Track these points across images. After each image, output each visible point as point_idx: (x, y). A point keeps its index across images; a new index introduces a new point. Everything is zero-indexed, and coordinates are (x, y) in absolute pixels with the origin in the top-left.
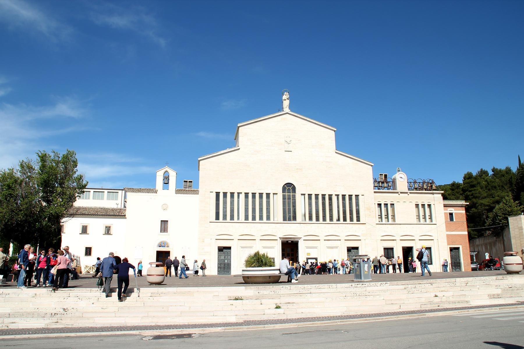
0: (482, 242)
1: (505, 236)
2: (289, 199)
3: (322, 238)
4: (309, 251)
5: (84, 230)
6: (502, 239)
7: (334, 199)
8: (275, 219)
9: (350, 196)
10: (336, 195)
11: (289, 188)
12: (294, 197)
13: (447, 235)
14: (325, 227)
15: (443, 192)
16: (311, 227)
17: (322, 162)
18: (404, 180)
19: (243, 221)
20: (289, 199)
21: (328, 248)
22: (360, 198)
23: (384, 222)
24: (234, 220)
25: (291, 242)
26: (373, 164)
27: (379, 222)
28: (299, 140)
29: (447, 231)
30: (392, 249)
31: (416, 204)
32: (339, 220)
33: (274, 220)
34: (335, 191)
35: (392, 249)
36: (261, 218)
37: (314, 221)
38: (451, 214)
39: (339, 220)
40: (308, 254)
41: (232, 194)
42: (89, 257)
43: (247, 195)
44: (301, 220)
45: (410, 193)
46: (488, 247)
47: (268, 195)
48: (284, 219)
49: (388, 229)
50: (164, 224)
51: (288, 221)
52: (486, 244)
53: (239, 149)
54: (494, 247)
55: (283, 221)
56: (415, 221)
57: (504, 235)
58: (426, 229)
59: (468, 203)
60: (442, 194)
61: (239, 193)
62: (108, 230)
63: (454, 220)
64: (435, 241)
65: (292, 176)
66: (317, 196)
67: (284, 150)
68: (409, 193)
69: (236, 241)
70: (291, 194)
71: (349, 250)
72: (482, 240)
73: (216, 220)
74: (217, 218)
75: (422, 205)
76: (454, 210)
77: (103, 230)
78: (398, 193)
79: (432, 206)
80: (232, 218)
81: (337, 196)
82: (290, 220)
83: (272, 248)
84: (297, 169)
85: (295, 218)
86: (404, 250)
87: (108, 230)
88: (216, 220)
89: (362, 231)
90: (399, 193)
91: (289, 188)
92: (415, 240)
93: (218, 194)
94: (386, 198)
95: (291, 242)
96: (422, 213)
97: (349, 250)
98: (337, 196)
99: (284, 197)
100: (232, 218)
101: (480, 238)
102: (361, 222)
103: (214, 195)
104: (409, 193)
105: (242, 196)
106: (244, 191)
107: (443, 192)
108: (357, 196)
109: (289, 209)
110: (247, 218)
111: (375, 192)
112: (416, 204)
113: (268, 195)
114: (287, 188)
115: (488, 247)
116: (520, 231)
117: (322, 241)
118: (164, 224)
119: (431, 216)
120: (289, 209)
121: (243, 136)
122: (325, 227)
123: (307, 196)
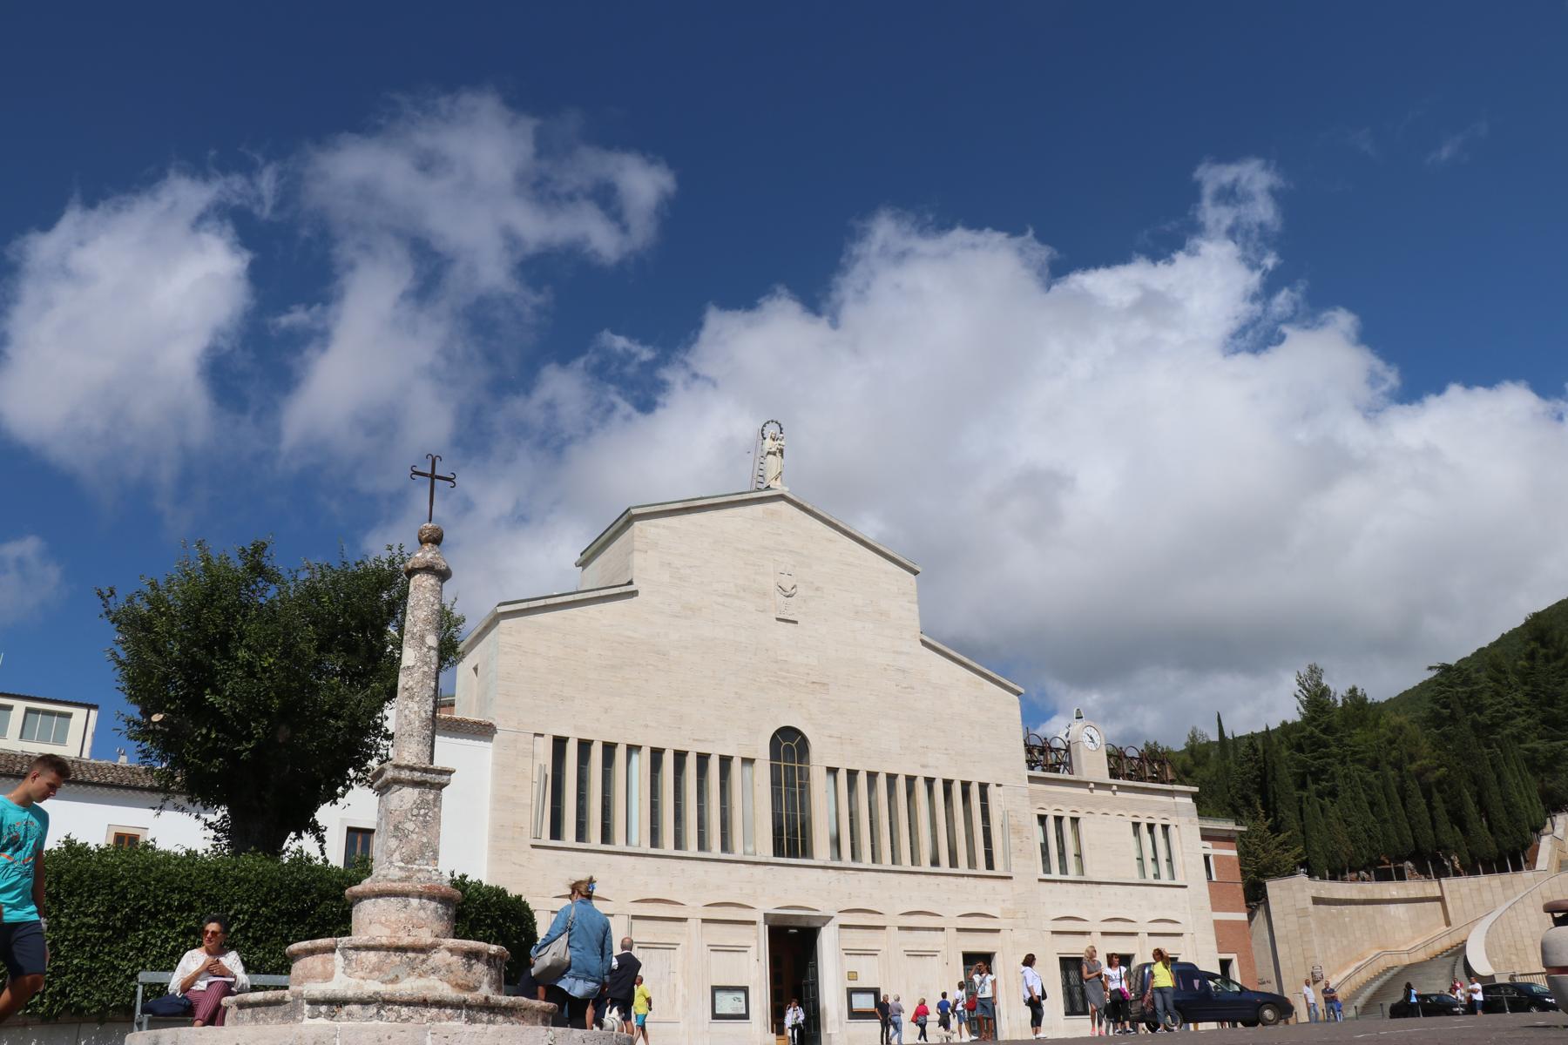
3: (892, 920)
4: (853, 963)
9: (680, 757)
13: (1217, 924)
14: (899, 883)
15: (1196, 789)
16: (859, 881)
18: (1094, 749)
19: (646, 847)
22: (992, 791)
23: (1150, 879)
25: (795, 931)
26: (1022, 690)
29: (1214, 909)
31: (1134, 823)
36: (581, 835)
37: (617, 843)
40: (853, 976)
41: (609, 749)
43: (657, 754)
44: (828, 856)
45: (1122, 788)
47: (725, 761)
48: (778, 851)
49: (1065, 900)
53: (634, 594)
55: (775, 855)
58: (1159, 903)
59: (1244, 829)
60: (1195, 797)
65: (800, 704)
66: (584, 746)
67: (774, 616)
68: (1115, 788)
69: (694, 925)
71: (970, 959)
74: (556, 832)
75: (1072, 818)
79: (1172, 830)
81: (930, 781)
83: (740, 950)
84: (814, 682)
85: (807, 852)
86: (814, 958)
89: (1004, 901)
90: (1092, 785)
92: (1089, 933)
93: (559, 744)
94: (1060, 801)
95: (795, 931)
96: (1148, 855)
97: (970, 959)
98: (930, 781)
99: (775, 770)
100: (606, 836)
102: (999, 869)
103: (545, 750)
104: (1115, 788)
105: (642, 762)
106: (648, 741)
107: (1196, 789)
108: (983, 787)
111: (1032, 779)
112: (1134, 823)
113: (725, 761)
114: (793, 745)
117: (893, 932)
121: (646, 552)
123: (842, 777)
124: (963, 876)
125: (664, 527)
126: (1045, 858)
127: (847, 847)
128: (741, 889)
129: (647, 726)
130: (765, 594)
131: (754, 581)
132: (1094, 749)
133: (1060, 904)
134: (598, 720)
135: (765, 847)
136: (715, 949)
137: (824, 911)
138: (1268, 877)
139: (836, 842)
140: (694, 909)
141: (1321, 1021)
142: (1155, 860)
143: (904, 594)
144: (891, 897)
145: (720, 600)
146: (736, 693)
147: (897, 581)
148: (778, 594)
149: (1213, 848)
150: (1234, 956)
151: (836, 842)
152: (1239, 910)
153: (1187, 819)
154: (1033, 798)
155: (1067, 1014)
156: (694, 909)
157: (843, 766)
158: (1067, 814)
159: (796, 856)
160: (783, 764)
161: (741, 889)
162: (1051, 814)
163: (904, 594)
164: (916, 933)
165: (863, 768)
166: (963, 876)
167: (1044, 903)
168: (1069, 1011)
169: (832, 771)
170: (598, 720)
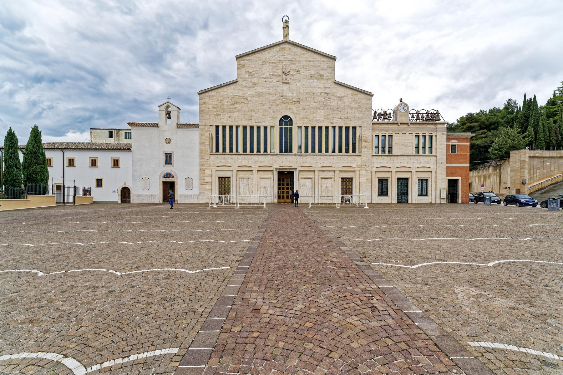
0: (476, 175)
1: (503, 169)
2: (286, 131)
3: (316, 169)
5: (94, 163)
6: (499, 172)
7: (331, 131)
8: (272, 151)
10: (332, 127)
11: (286, 120)
12: (291, 129)
17: (320, 94)
18: (404, 112)
20: (286, 131)
21: (322, 178)
24: (219, 152)
27: (298, 152)
28: (297, 71)
30: (387, 180)
32: (334, 151)
33: (271, 152)
34: (332, 123)
35: (387, 180)
36: (347, 151)
38: (454, 147)
39: (334, 151)
42: (99, 189)
44: (296, 152)
46: (482, 179)
48: (281, 151)
49: (385, 161)
50: (168, 159)
51: (289, 152)
52: (480, 176)
54: (489, 178)
56: (413, 152)
57: (502, 168)
61: (237, 127)
62: (116, 163)
63: (456, 153)
64: (433, 173)
70: (288, 126)
72: (476, 173)
73: (325, 153)
76: (458, 142)
77: (111, 163)
78: (398, 124)
79: (434, 138)
80: (354, 151)
81: (334, 128)
82: (286, 151)
85: (291, 151)
87: (116, 163)
88: (325, 153)
91: (286, 120)
93: (217, 128)
98: (334, 128)
99: (281, 129)
101: (474, 172)
102: (434, 154)
103: (213, 130)
105: (241, 130)
108: (354, 128)
109: (286, 142)
110: (245, 150)
115: (482, 179)
116: (522, 164)
118: (168, 159)
119: (431, 147)
120: (286, 142)
122: (320, 158)
123: (303, 129)
124: (337, 155)
125: (247, 60)
126: (307, 146)
127: (306, 149)
128: (269, 162)
129: (241, 120)
130: (279, 76)
131: (276, 72)
132: (404, 112)
133: (380, 163)
134: (227, 120)
135: (277, 149)
136: (261, 178)
137: (295, 167)
138: (511, 150)
139: (300, 147)
140: (255, 168)
141: (460, 204)
142: (424, 147)
143: (329, 68)
144: (317, 162)
145: (264, 80)
146: (269, 107)
147: (327, 64)
148: (283, 75)
149: (458, 142)
150: (460, 178)
151: (300, 147)
152: (466, 163)
153: (441, 133)
154: (373, 130)
155: (378, 195)
156: (255, 168)
157: (303, 126)
158: (387, 134)
159: (287, 152)
160: (284, 126)
161: (269, 162)
162: (380, 134)
163: (329, 68)
164: (325, 172)
165: (310, 125)
166: (337, 155)
167: (374, 163)
168: (380, 193)
169: (300, 127)
170: (227, 120)
